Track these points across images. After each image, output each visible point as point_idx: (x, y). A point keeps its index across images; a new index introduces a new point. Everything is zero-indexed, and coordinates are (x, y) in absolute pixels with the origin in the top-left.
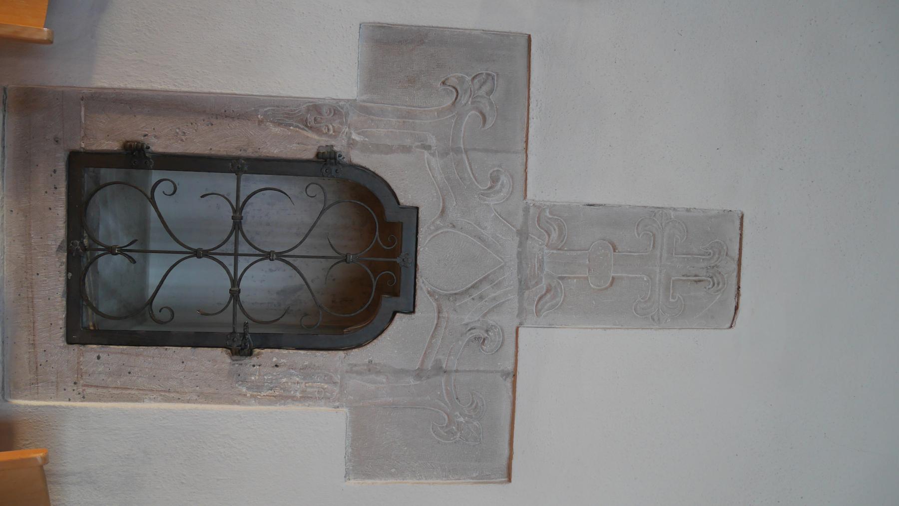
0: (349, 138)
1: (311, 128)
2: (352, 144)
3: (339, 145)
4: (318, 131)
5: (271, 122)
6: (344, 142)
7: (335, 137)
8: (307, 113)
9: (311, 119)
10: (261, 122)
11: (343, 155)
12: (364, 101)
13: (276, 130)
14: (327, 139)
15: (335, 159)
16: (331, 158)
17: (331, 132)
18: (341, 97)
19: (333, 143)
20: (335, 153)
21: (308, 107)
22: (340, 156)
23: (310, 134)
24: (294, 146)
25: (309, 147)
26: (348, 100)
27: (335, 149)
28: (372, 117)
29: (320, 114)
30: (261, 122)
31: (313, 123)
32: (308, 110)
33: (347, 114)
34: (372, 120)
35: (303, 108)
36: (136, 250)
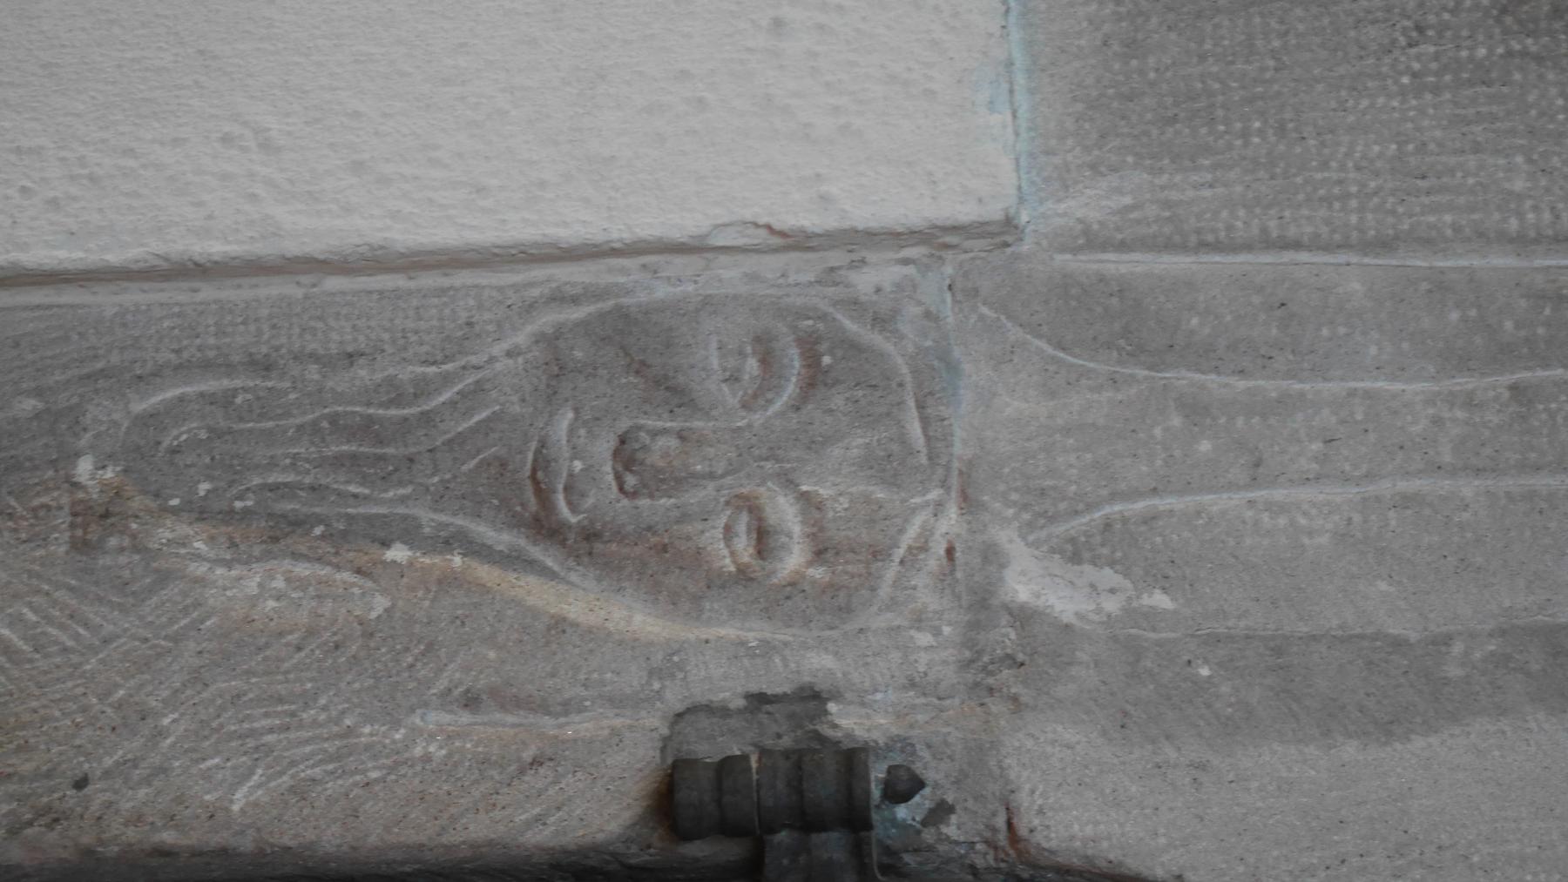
0: (982, 603)
1: (588, 544)
2: (1009, 660)
3: (880, 686)
4: (655, 561)
5: (201, 512)
6: (934, 650)
7: (835, 604)
8: (551, 398)
9: (580, 448)
10: (97, 519)
11: (933, 771)
12: (1091, 240)
13: (257, 588)
14: (755, 632)
15: (855, 819)
16: (808, 822)
17: (794, 559)
18: (863, 216)
19: (820, 664)
20: (852, 759)
21: (550, 339)
22: (903, 787)
23: (580, 600)
24: (432, 731)
25: (580, 727)
26: (935, 238)
27: (848, 722)
28: (1183, 378)
29: (672, 391)
30: (97, 519)
31: (603, 496)
32: (556, 369)
33: (935, 376)
34: (1196, 410)
35: (505, 355)
36: (1214, 231)
